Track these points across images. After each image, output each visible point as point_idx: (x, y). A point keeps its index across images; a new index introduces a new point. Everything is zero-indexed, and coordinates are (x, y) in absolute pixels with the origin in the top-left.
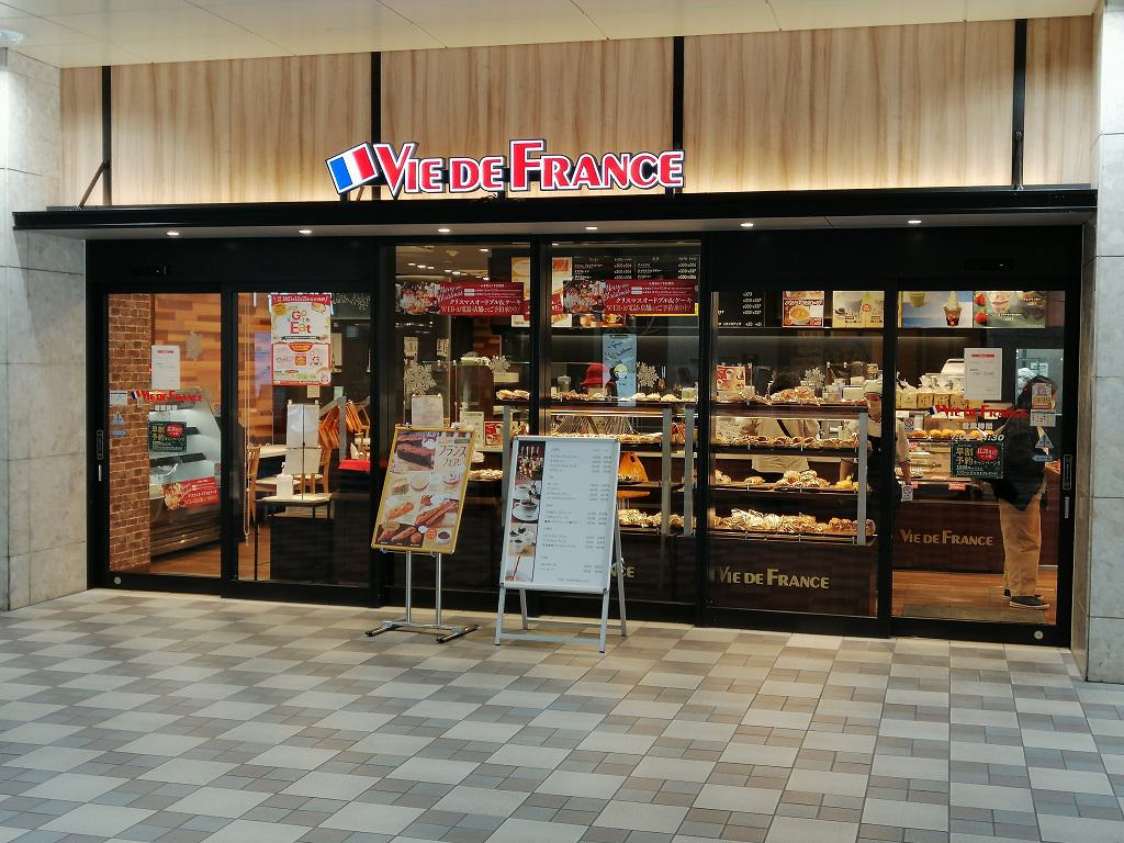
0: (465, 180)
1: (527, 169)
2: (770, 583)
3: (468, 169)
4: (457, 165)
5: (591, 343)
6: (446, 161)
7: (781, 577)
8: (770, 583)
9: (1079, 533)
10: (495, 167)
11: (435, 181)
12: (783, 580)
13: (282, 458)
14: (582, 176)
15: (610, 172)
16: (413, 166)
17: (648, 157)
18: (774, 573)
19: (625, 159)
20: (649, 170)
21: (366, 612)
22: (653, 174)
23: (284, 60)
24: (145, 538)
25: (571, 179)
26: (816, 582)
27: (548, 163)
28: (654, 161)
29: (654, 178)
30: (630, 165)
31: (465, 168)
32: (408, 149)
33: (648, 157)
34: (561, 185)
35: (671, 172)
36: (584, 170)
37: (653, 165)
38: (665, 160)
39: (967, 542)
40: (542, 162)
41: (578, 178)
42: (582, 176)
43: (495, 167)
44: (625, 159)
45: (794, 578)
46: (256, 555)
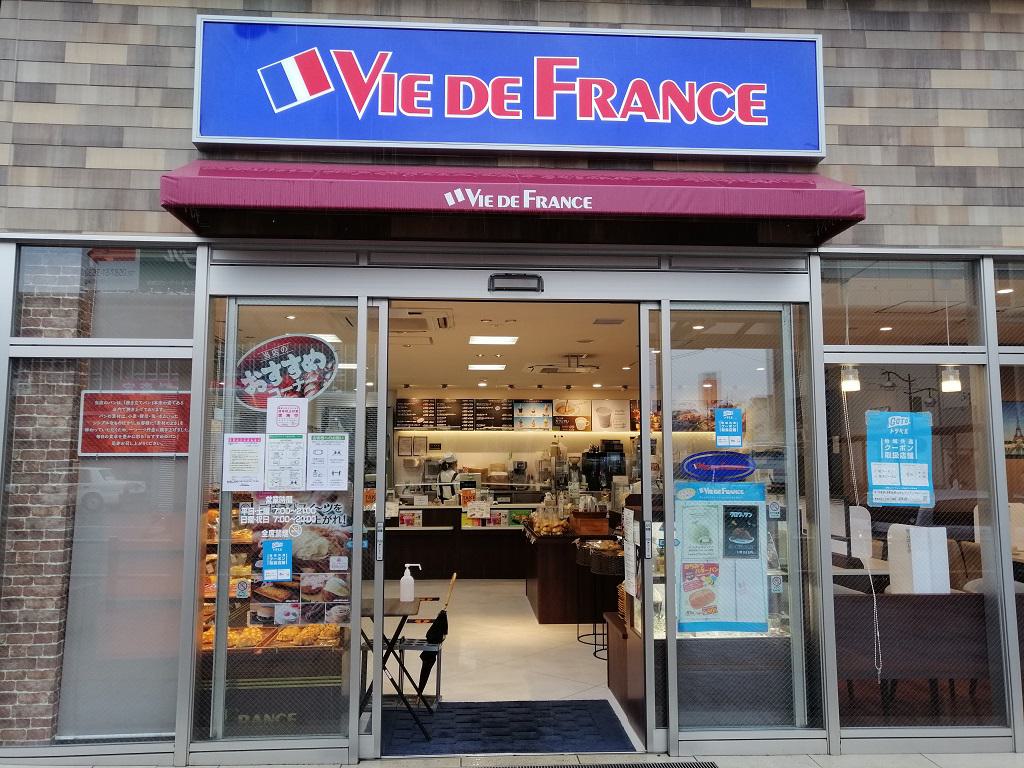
1: (556, 92)
4: (454, 84)
6: (439, 81)
7: (538, 198)
12: (541, 203)
15: (671, 101)
16: (388, 83)
18: (531, 195)
19: (691, 87)
20: (723, 104)
22: (729, 109)
26: (579, 203)
27: (586, 89)
28: (730, 92)
31: (467, 89)
32: (383, 57)
33: (725, 88)
37: (728, 96)
38: (744, 93)
40: (577, 84)
41: (628, 108)
42: (632, 105)
43: (510, 90)
45: (554, 199)
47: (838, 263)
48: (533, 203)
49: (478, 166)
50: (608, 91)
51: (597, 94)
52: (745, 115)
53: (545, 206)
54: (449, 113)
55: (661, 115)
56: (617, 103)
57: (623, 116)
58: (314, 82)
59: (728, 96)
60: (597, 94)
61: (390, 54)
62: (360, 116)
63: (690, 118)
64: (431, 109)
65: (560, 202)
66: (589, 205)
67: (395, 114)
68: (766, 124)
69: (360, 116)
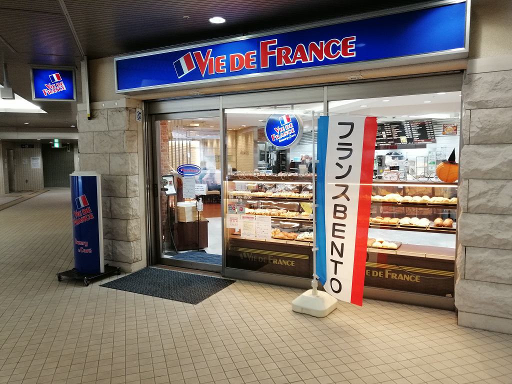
2: (387, 276)
5: (229, 231)
7: (393, 274)
8: (387, 276)
20: (335, 49)
21: (357, 102)
22: (338, 51)
23: (104, 239)
24: (26, 149)
26: (413, 278)
27: (280, 52)
28: (338, 43)
34: (173, 248)
36: (299, 53)
37: (338, 45)
38: (345, 43)
39: (402, 278)
40: (276, 51)
42: (298, 56)
48: (390, 276)
50: (288, 51)
52: (345, 53)
53: (396, 278)
54: (267, 66)
55: (308, 59)
58: (189, 66)
59: (338, 45)
64: (313, 61)
65: (403, 277)
66: (418, 280)
67: (283, 65)
68: (355, 56)
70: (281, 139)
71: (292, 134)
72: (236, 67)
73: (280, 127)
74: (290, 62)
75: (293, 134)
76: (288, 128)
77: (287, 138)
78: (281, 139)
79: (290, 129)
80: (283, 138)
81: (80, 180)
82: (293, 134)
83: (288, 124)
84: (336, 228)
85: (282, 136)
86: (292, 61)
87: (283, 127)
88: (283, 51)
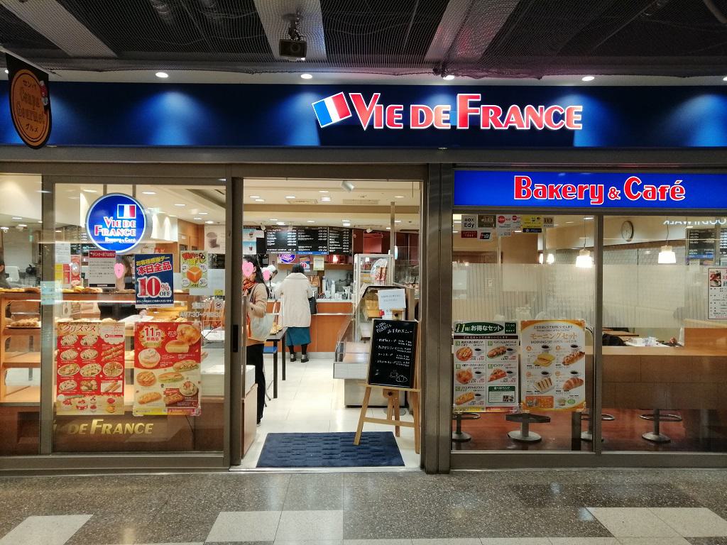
0: (422, 121)
3: (157, 278)
9: (619, 218)
10: (397, 112)
11: (397, 121)
13: (257, 467)
14: (511, 120)
17: (555, 108)
19: (542, 109)
25: (503, 122)
28: (562, 111)
29: (562, 123)
30: (544, 113)
31: (421, 113)
35: (402, 109)
37: (561, 113)
42: (511, 120)
43: (397, 112)
44: (542, 109)
46: (391, 189)
47: (340, 203)
49: (248, 148)
50: (497, 112)
51: (492, 114)
54: (413, 126)
56: (502, 119)
57: (506, 126)
59: (561, 113)
60: (492, 114)
61: (380, 94)
62: (365, 129)
63: (540, 127)
68: (402, 128)
69: (365, 129)
70: (109, 237)
71: (130, 237)
72: (420, 124)
73: (115, 218)
74: (501, 126)
75: (133, 238)
76: (127, 226)
77: (120, 241)
78: (109, 237)
79: (130, 228)
80: (113, 237)
81: (44, 192)
82: (133, 238)
83: (130, 220)
84: (366, 416)
85: (112, 234)
86: (503, 125)
87: (119, 222)
88: (491, 110)
